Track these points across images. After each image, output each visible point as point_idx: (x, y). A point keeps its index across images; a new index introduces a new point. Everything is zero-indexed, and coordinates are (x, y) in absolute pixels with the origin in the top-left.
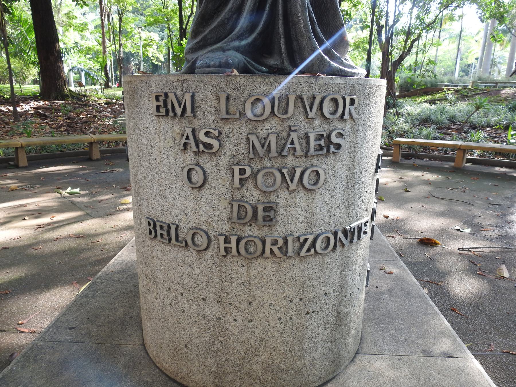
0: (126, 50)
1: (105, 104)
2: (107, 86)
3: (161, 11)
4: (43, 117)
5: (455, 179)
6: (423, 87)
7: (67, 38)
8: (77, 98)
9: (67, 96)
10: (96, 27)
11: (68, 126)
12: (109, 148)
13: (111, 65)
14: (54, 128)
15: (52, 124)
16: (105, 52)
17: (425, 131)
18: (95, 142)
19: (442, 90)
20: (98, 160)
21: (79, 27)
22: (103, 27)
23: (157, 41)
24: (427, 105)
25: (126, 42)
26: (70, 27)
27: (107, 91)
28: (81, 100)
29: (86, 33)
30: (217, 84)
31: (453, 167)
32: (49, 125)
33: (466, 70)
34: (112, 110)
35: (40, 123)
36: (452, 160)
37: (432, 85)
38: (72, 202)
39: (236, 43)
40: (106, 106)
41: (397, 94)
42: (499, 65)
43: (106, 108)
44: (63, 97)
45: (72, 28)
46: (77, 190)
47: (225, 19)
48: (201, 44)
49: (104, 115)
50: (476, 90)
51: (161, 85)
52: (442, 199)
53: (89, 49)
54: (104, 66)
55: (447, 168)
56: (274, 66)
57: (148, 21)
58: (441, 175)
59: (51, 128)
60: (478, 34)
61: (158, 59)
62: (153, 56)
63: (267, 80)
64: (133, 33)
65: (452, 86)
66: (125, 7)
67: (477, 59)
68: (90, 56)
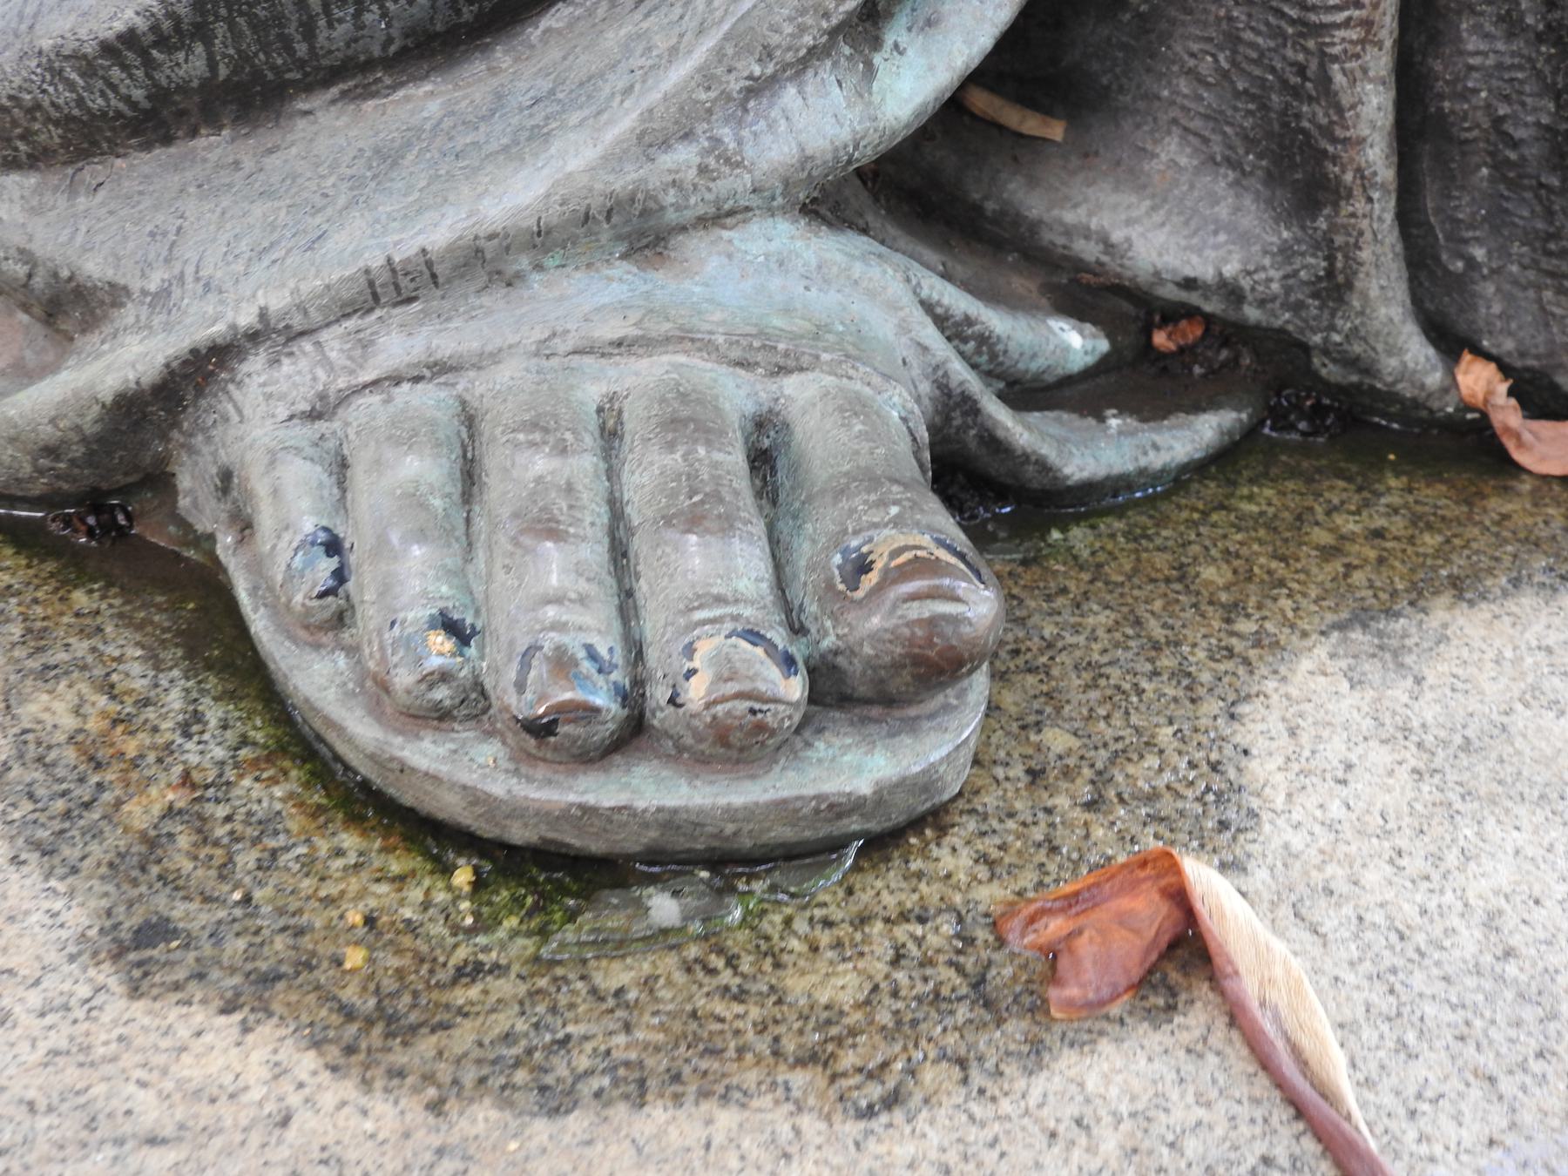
48: (192, 65)
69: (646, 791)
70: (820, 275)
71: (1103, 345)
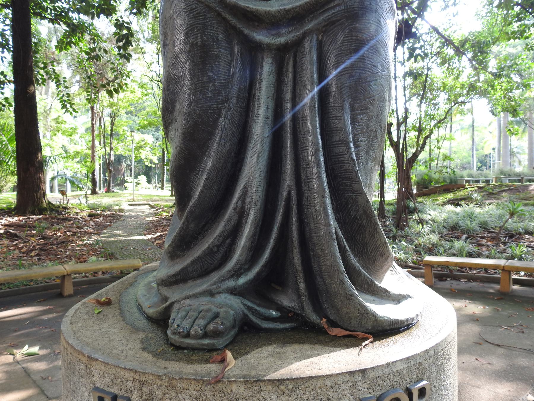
0: (117, 153)
1: (89, 216)
2: (94, 192)
3: (156, 114)
4: (12, 237)
5: (507, 311)
6: (443, 184)
7: (54, 142)
8: (57, 211)
9: (45, 209)
10: (87, 130)
11: (41, 249)
12: (85, 279)
13: (100, 168)
14: (23, 253)
15: (22, 247)
16: (93, 156)
17: (458, 244)
18: (68, 275)
19: (464, 187)
20: (70, 296)
21: (67, 131)
22: (93, 131)
23: (151, 143)
24: (450, 208)
25: (117, 145)
26: (58, 131)
27: (93, 200)
28: (60, 214)
29: (76, 137)
30: (197, 394)
31: (498, 291)
32: (19, 248)
33: (484, 162)
34: (96, 223)
35: (7, 247)
36: (497, 281)
37: (451, 182)
38: (26, 371)
39: (231, 283)
40: (88, 219)
41: (415, 191)
42: (518, 155)
43: (89, 221)
44: (41, 211)
45: (60, 132)
46: (35, 349)
47: (214, 246)
48: (179, 277)
49: (86, 232)
50: (501, 186)
51: (107, 379)
52: (499, 346)
53: (78, 153)
54: (91, 171)
55: (491, 293)
56: (288, 308)
57: (142, 124)
58: (488, 306)
59: (20, 252)
60: (490, 124)
61: (151, 162)
62: (146, 158)
63: (282, 387)
64: (126, 136)
65: (473, 181)
66: (119, 111)
67: (494, 149)
68: (78, 159)
69: (188, 341)
70: (230, 299)
71: (280, 314)
